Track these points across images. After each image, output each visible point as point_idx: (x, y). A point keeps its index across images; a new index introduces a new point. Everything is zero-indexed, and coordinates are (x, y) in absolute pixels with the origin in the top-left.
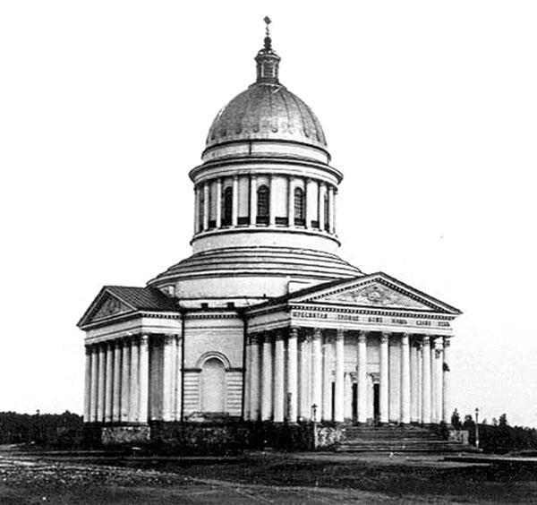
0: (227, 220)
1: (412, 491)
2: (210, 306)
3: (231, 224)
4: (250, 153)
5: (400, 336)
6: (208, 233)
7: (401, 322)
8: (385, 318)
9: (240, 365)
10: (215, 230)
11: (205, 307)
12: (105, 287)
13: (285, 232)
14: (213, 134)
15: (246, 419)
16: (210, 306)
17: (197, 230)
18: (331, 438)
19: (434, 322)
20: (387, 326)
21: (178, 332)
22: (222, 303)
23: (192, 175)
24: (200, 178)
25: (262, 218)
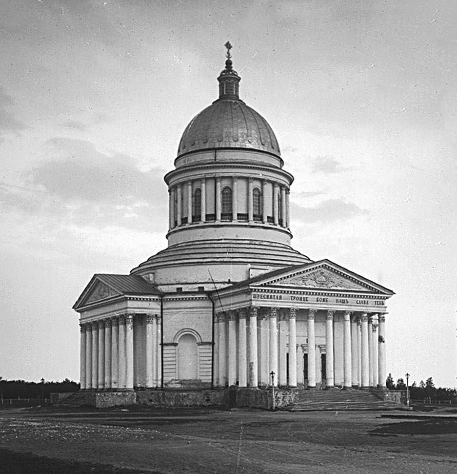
9: (211, 341)
10: (187, 226)
13: (246, 226)
16: (206, 289)
17: (172, 226)
24: (173, 181)
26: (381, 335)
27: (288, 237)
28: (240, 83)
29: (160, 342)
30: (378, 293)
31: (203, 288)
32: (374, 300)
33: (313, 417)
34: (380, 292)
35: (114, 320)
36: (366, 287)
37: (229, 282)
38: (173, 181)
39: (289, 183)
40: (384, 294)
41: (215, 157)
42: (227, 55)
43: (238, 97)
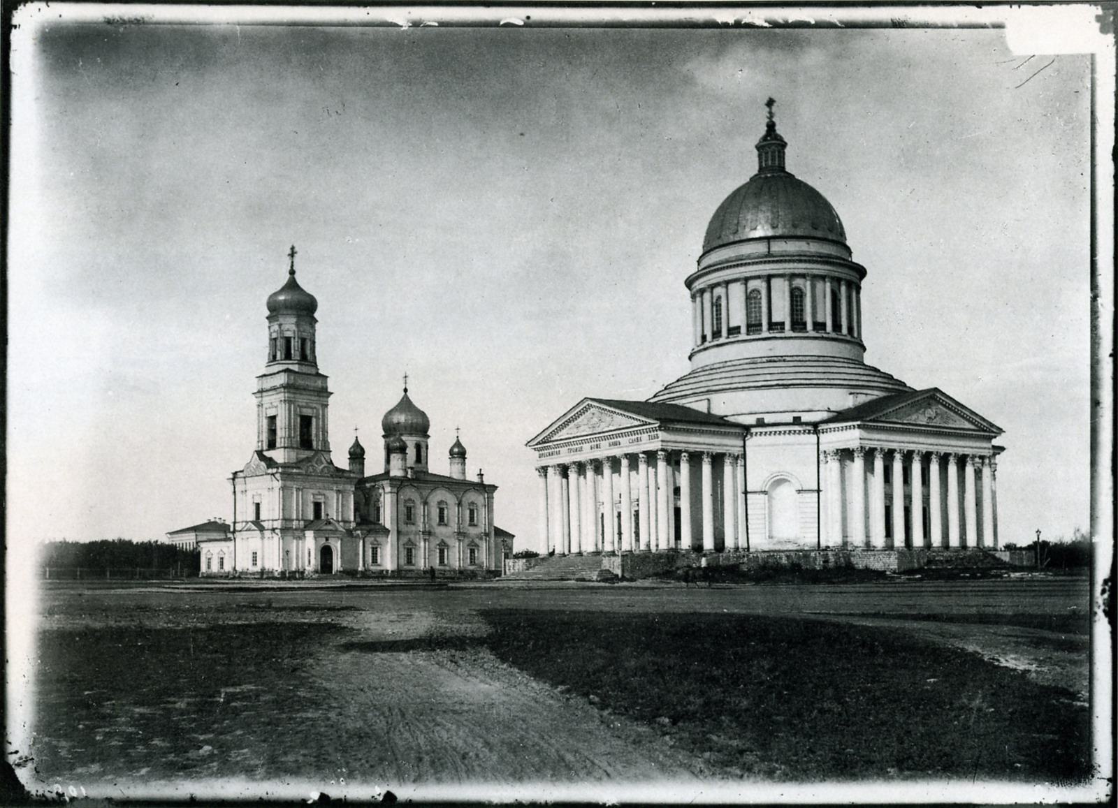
0: (717, 334)
1: (679, 614)
2: (803, 420)
3: (720, 336)
4: (769, 252)
5: (678, 453)
6: (713, 344)
7: (615, 444)
8: (622, 440)
9: (816, 488)
10: (722, 340)
11: (761, 423)
12: (936, 390)
13: (781, 338)
14: (708, 240)
15: (653, 549)
16: (803, 420)
17: (699, 342)
18: (516, 568)
19: (645, 437)
20: (605, 451)
21: (737, 451)
22: (789, 418)
23: (689, 283)
24: (698, 285)
25: (755, 325)
26: (542, 480)
27: (858, 349)
28: (787, 150)
29: (740, 488)
30: (646, 425)
31: (800, 418)
32: (646, 435)
33: (874, 600)
34: (986, 430)
35: (663, 453)
36: (973, 424)
37: (829, 410)
38: (698, 285)
39: (858, 276)
40: (650, 424)
41: (769, 249)
42: (768, 115)
43: (784, 168)
